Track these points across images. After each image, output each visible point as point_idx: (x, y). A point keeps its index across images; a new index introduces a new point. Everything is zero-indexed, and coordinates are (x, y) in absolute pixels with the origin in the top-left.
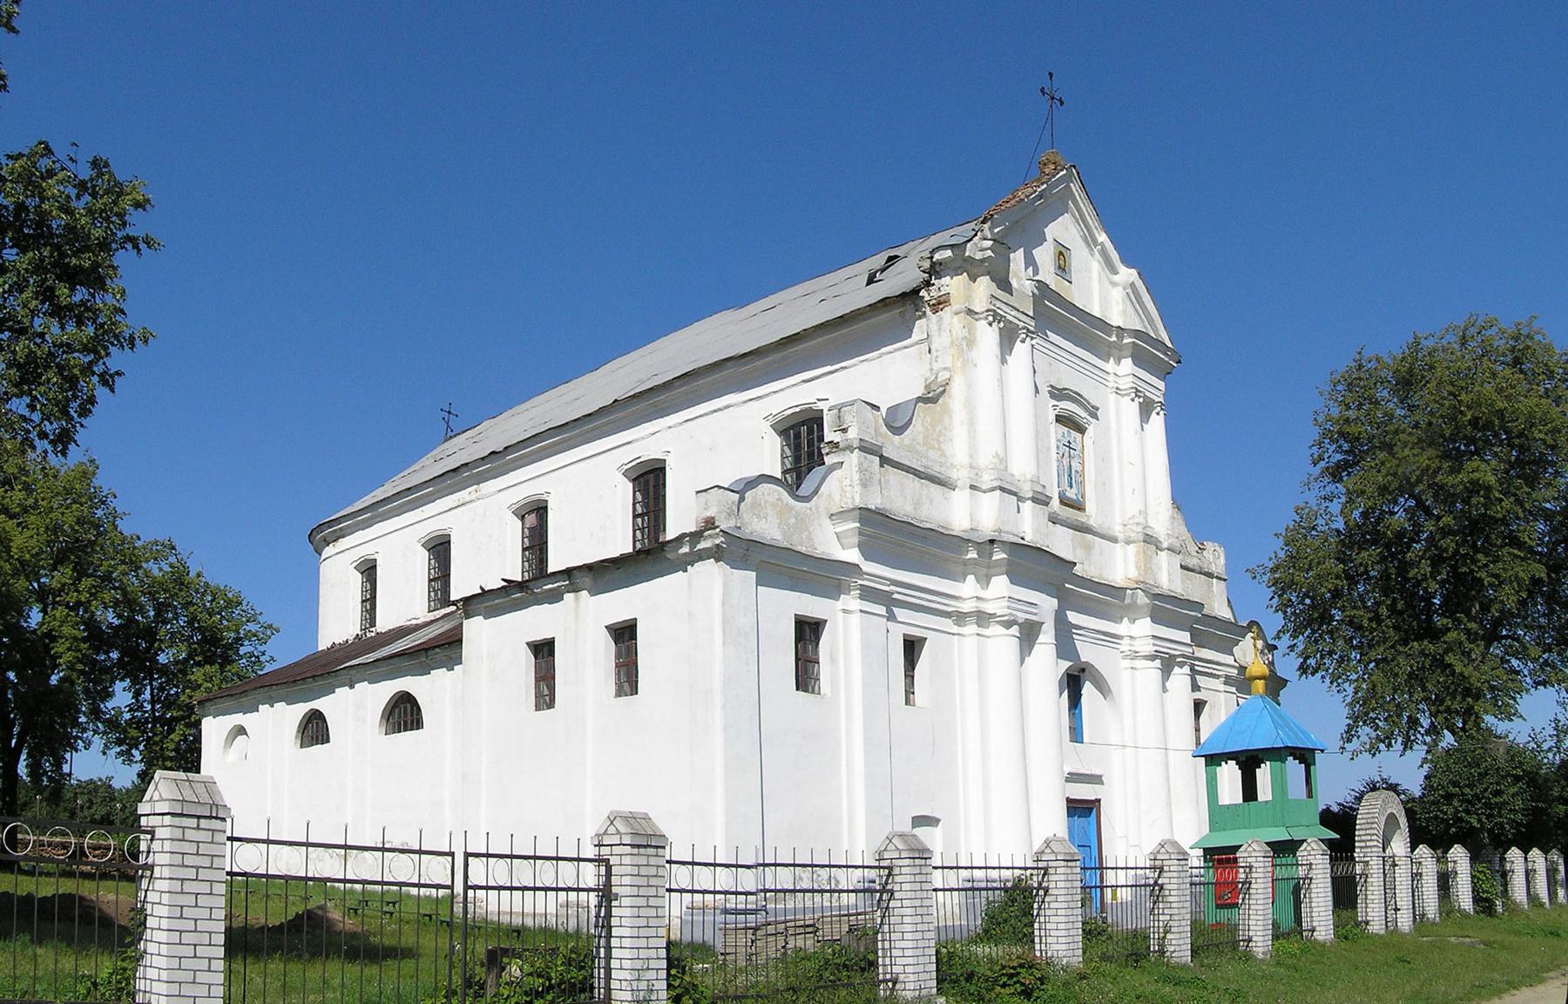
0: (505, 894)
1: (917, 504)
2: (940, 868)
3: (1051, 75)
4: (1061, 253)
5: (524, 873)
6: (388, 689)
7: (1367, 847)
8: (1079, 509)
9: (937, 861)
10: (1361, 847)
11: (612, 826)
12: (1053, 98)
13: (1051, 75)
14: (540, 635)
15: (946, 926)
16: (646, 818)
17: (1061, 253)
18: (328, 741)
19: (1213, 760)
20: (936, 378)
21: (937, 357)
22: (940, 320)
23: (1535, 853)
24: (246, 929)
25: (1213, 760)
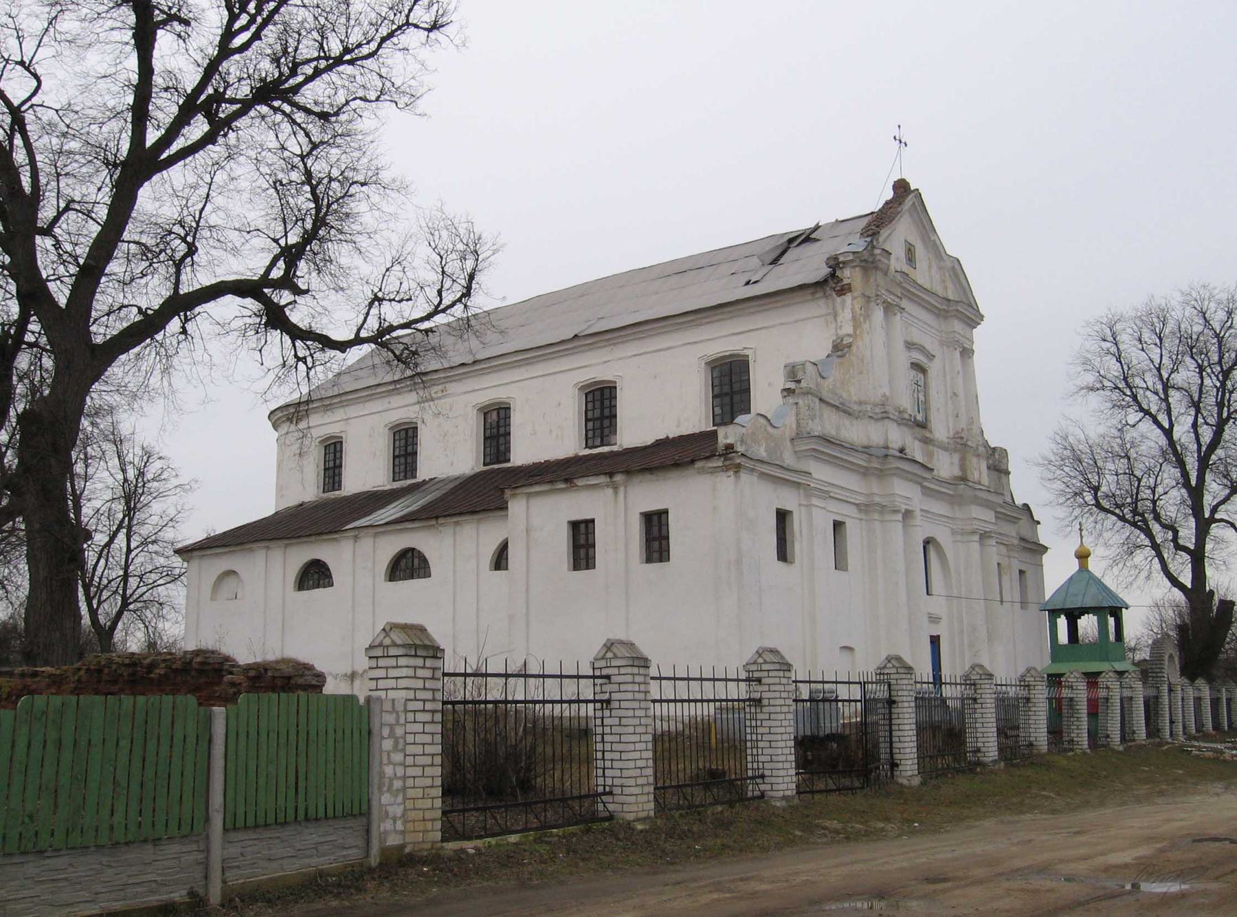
0: (672, 705)
1: (838, 429)
2: (665, 679)
3: (899, 126)
4: (909, 250)
5: (682, 691)
6: (391, 546)
7: (1157, 677)
8: (924, 428)
9: (653, 672)
10: (1152, 677)
11: (387, 638)
12: (901, 142)
13: (899, 126)
14: (1023, 569)
15: (561, 717)
16: (422, 630)
17: (909, 250)
18: (332, 585)
19: (1054, 613)
20: (842, 341)
21: (841, 326)
22: (844, 301)
23: (1200, 682)
24: (805, 737)
25: (1054, 613)
